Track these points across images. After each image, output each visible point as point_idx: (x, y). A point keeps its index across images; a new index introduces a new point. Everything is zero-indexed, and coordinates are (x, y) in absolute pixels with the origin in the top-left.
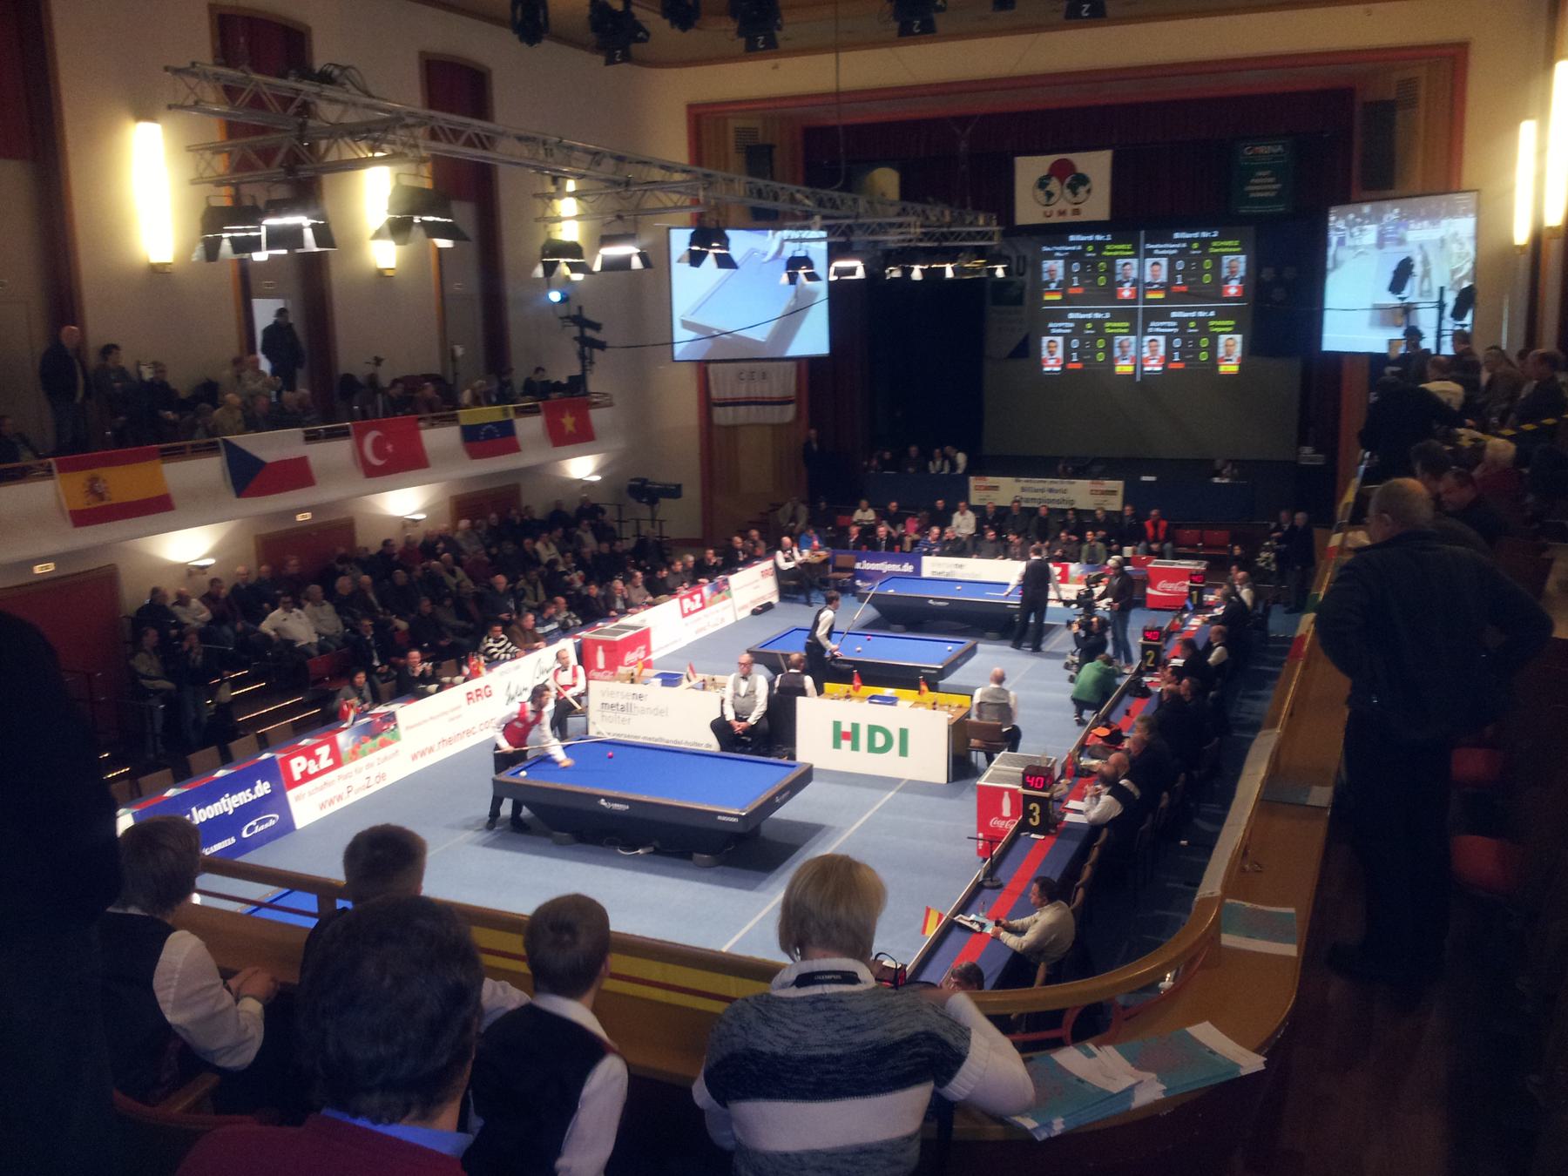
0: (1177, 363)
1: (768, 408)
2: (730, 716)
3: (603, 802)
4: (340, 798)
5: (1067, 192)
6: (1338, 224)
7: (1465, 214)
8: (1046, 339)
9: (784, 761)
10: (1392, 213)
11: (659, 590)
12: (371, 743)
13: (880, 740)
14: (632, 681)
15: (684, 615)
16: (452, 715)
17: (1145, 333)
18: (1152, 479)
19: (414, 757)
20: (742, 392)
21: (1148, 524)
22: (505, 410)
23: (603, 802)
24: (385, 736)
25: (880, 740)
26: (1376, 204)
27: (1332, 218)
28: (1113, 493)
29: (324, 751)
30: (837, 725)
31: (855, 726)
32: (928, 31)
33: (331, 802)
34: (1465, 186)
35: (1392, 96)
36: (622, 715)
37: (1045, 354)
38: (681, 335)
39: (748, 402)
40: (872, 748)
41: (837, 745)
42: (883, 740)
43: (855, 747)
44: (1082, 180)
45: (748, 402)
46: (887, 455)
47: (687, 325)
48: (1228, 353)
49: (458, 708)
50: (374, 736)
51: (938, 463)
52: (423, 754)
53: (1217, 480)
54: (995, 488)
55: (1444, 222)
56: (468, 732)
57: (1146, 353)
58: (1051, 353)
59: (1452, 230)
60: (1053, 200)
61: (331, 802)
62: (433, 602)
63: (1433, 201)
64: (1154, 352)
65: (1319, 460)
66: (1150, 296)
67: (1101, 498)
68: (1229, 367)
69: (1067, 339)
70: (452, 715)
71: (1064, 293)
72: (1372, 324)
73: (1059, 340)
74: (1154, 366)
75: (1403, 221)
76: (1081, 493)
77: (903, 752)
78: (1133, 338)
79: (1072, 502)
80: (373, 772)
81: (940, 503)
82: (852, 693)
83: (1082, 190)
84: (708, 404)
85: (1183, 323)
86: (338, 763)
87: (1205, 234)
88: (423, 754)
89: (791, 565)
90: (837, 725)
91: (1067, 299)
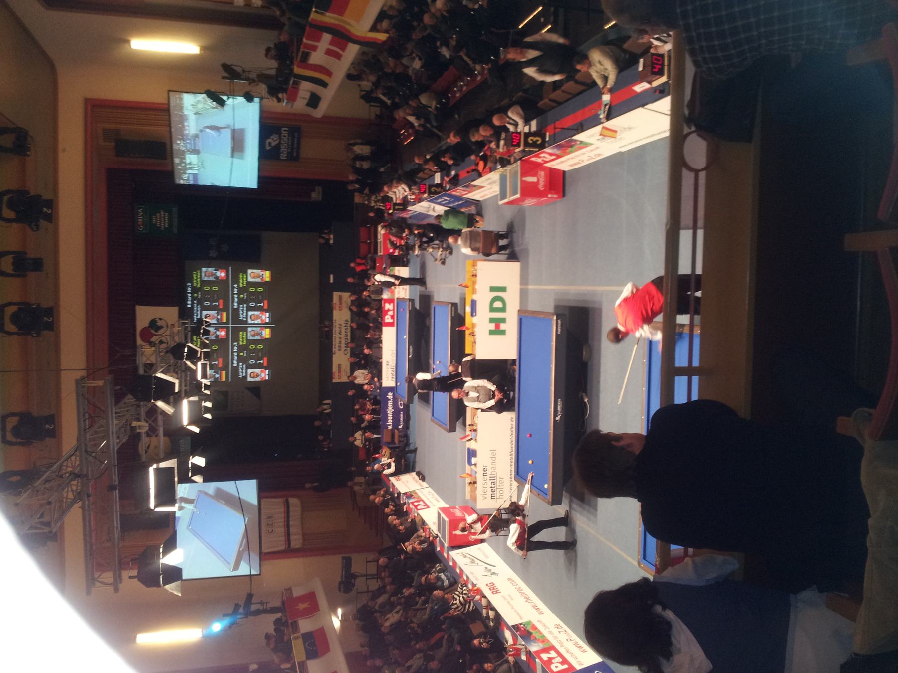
0: (265, 304)
1: (291, 514)
2: (492, 403)
3: (558, 418)
4: (576, 644)
5: (160, 332)
6: (185, 178)
7: (181, 99)
8: (249, 379)
9: (517, 368)
10: (179, 145)
11: (415, 526)
12: (534, 633)
13: (498, 304)
14: (475, 482)
15: (428, 507)
16: (509, 599)
17: (246, 322)
18: (332, 276)
19: (541, 613)
20: (281, 530)
21: (358, 269)
22: (295, 638)
23: (558, 418)
24: (529, 628)
25: (498, 304)
26: (174, 155)
27: (182, 182)
28: (340, 297)
29: (545, 656)
30: (492, 332)
31: (492, 320)
32: (51, 204)
33: (580, 647)
34: (165, 101)
35: (113, 144)
36: (498, 483)
37: (258, 379)
38: (244, 570)
39: (288, 526)
40: (503, 309)
41: (503, 332)
42: (498, 304)
43: (503, 320)
44: (153, 323)
45: (288, 526)
46: (321, 438)
47: (236, 567)
48: (259, 276)
49: (504, 597)
50: (530, 634)
51: (325, 407)
52: (538, 609)
53: (331, 242)
54: (339, 366)
55: (186, 112)
56: (520, 590)
57: (258, 321)
58: (258, 376)
59: (190, 108)
60: (163, 339)
61: (580, 647)
62: (433, 660)
63: (174, 119)
64: (258, 317)
65: (319, 189)
66: (225, 320)
67: (344, 304)
68: (267, 275)
69: (249, 367)
70: (509, 599)
71: (222, 369)
72: (242, 158)
73: (250, 371)
74: (266, 317)
75: (183, 137)
76: (341, 316)
77: (503, 289)
78: (250, 329)
79: (347, 321)
80: (556, 631)
81: (350, 393)
82: (470, 331)
83: (159, 323)
84: (289, 552)
85: (241, 302)
86: (553, 648)
87: (189, 290)
88: (538, 609)
89: (393, 464)
90: (492, 332)
91: (225, 367)
